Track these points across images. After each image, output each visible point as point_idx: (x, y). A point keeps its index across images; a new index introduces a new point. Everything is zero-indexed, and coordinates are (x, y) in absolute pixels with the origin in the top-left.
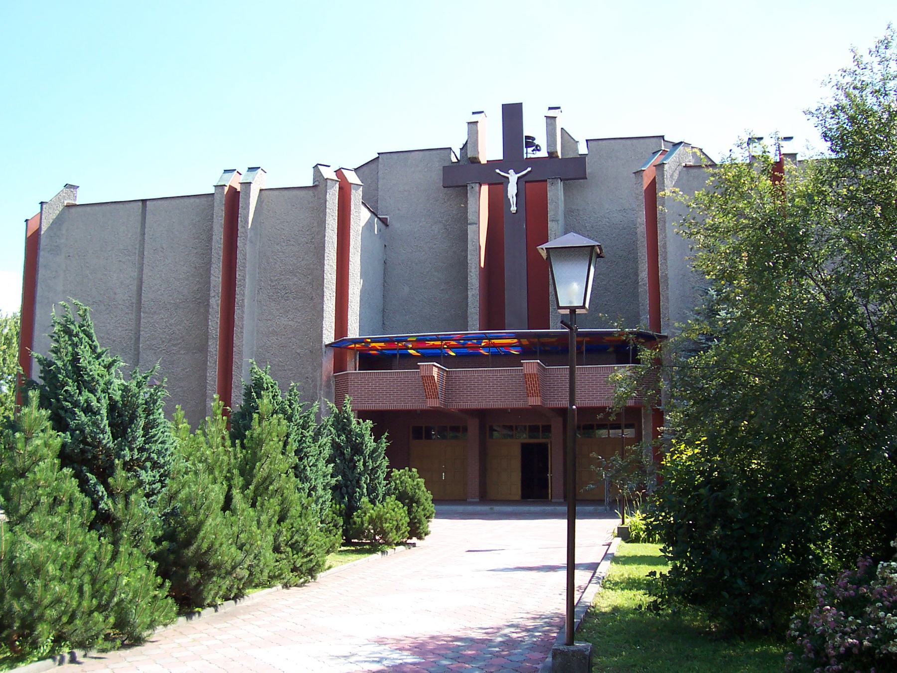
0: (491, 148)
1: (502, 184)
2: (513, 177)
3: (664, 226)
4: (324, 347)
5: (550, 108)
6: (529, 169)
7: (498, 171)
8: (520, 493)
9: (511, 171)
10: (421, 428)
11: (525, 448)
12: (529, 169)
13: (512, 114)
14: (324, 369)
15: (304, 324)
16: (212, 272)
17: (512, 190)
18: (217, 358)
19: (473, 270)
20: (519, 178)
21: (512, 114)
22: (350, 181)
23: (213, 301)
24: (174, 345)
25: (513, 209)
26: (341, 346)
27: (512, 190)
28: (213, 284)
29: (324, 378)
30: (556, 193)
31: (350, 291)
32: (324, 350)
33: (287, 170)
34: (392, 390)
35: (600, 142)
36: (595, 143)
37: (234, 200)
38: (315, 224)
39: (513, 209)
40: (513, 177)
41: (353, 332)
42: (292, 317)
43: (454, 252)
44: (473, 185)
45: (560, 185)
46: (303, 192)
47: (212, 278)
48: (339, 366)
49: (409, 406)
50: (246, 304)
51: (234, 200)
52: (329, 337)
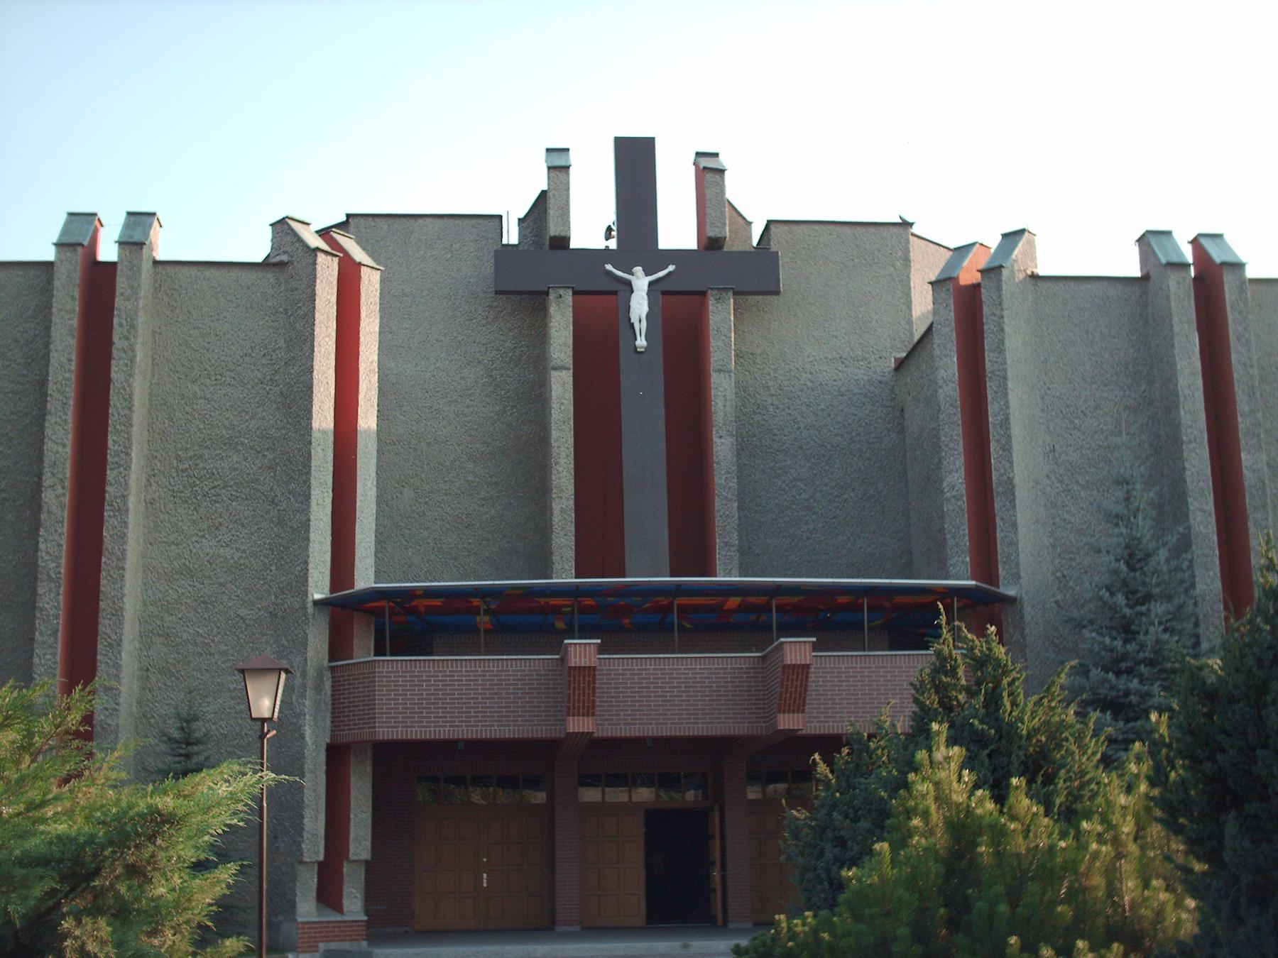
0: (591, 222)
1: (615, 293)
2: (641, 282)
4: (310, 605)
6: (671, 268)
9: (638, 270)
10: (302, 776)
11: (655, 819)
12: (671, 268)
13: (635, 160)
14: (310, 654)
16: (48, 432)
17: (639, 306)
18: (60, 623)
19: (562, 461)
20: (651, 284)
21: (635, 160)
22: (358, 259)
23: (48, 497)
25: (641, 342)
26: (346, 610)
27: (639, 306)
28: (49, 458)
29: (311, 672)
30: (721, 316)
31: (360, 490)
33: (214, 226)
35: (794, 227)
36: (785, 228)
37: (777, 293)
38: (282, 343)
39: (641, 342)
40: (641, 282)
41: (365, 578)
44: (562, 292)
46: (253, 275)
47: (48, 445)
48: (338, 647)
50: (131, 505)
51: (777, 293)
52: (319, 589)
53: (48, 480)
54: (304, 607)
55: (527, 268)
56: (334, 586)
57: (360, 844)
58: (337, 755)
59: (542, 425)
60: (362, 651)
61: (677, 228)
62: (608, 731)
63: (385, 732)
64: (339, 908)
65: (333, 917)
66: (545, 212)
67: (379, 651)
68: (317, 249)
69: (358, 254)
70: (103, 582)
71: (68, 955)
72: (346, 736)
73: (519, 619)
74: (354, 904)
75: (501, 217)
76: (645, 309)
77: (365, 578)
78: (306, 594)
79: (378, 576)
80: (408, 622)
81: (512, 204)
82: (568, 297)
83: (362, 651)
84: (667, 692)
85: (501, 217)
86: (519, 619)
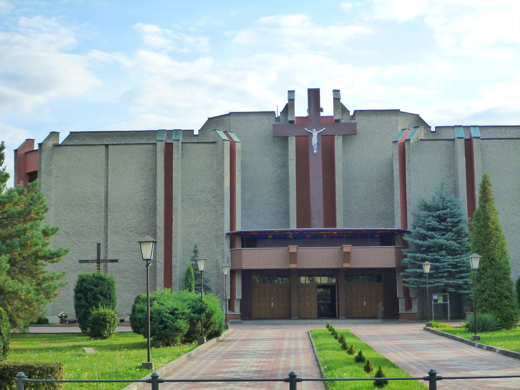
0: (301, 110)
3: (410, 173)
5: (336, 92)
6: (324, 129)
7: (306, 129)
8: (317, 314)
12: (324, 129)
13: (314, 95)
15: (210, 220)
17: (315, 140)
21: (314, 95)
22: (235, 140)
24: (131, 231)
27: (315, 140)
30: (338, 142)
32: (225, 236)
34: (259, 258)
42: (203, 216)
43: (278, 174)
44: (292, 137)
45: (341, 138)
48: (232, 245)
49: (276, 267)
52: (227, 229)
53: (158, 203)
54: (223, 235)
55: (283, 127)
56: (231, 230)
57: (238, 295)
58: (233, 272)
59: (287, 174)
60: (238, 246)
61: (327, 109)
62: (301, 267)
63: (245, 267)
64: (234, 311)
65: (232, 313)
66: (289, 108)
67: (243, 246)
68: (224, 140)
69: (235, 139)
70: (173, 229)
71: (1, 297)
72: (235, 268)
73: (279, 238)
74: (237, 310)
75: (274, 112)
76: (316, 141)
77: (238, 228)
78: (223, 231)
79: (242, 226)
80: (251, 239)
81: (277, 105)
82: (294, 138)
83: (238, 246)
84: (318, 256)
85: (274, 112)
86: (279, 238)
